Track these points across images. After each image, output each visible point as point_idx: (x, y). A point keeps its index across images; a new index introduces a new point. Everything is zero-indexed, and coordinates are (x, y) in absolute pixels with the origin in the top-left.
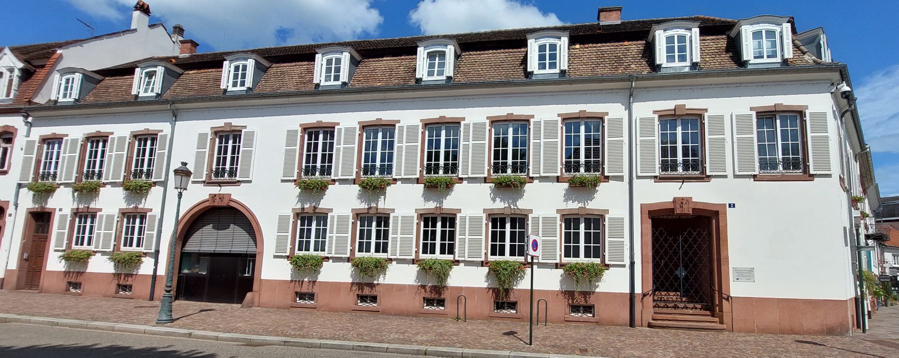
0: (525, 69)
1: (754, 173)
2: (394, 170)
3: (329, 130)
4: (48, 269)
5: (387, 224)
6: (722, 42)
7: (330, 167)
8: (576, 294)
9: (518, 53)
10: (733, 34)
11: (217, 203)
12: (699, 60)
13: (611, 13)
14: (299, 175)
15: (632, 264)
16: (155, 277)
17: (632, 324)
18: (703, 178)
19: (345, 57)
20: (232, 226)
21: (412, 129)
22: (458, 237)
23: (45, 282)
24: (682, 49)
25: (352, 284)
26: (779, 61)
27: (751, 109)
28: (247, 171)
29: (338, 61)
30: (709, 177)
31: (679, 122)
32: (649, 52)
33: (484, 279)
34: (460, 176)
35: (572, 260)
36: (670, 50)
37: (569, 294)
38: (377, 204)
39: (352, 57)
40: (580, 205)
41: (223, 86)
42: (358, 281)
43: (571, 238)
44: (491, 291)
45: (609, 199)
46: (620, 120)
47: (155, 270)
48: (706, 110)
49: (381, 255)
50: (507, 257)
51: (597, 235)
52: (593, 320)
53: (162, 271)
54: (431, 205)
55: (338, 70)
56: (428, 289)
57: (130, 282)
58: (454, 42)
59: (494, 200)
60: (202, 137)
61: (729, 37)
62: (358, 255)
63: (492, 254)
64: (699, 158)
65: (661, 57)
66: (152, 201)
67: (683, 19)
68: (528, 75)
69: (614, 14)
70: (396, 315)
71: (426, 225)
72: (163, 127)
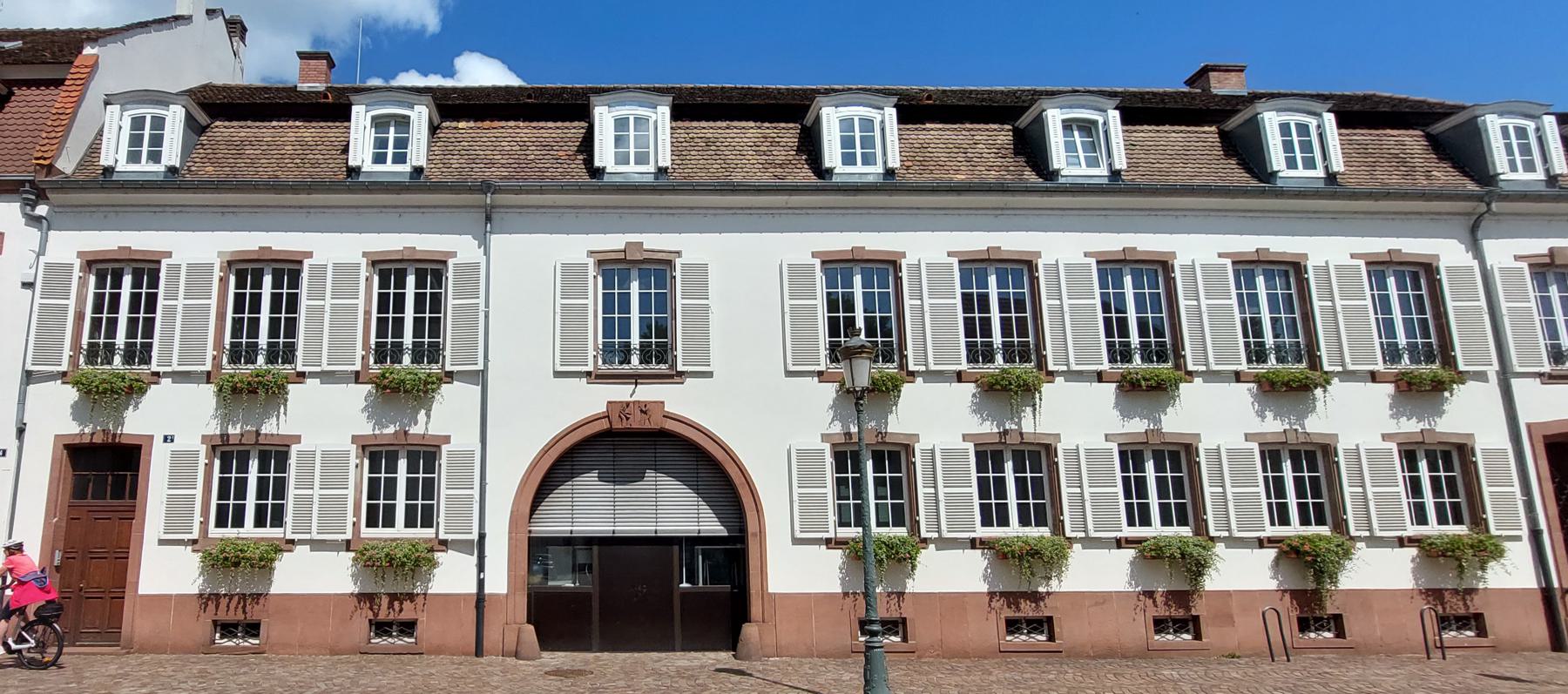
0: (589, 161)
1: (818, 368)
2: (155, 354)
3: (146, 266)
4: (774, 586)
5: (282, 465)
6: (1003, 135)
7: (148, 347)
8: (1447, 596)
9: (576, 129)
10: (1024, 120)
11: (637, 422)
12: (897, 165)
13: (1227, 75)
14: (74, 361)
15: (1535, 535)
16: (480, 599)
17: (479, 652)
18: (671, 376)
19: (175, 117)
20: (650, 474)
21: (199, 272)
22: (292, 491)
23: (134, 623)
24: (867, 142)
25: (991, 595)
26: (1106, 173)
27: (814, 255)
28: (701, 348)
29: (159, 123)
30: (681, 374)
31: (634, 273)
32: (810, 144)
33: (1269, 573)
34: (448, 368)
35: (995, 532)
36: (847, 142)
37: (1435, 595)
38: (1019, 424)
39: (189, 117)
40: (1421, 426)
41: (105, 160)
42: (1001, 588)
43: (990, 489)
44: (1287, 597)
45: (1471, 414)
46: (476, 266)
47: (481, 583)
48: (679, 253)
49: (269, 532)
50: (249, 529)
51: (897, 484)
52: (905, 647)
53: (497, 582)
54: (1138, 426)
55: (157, 141)
56: (1159, 599)
57: (254, 612)
58: (428, 99)
59: (1262, 416)
60: (798, 273)
61: (1016, 131)
62: (367, 533)
63: (368, 525)
64: (668, 340)
65: (832, 155)
66: (448, 416)
67: (1303, 96)
68: (597, 173)
69: (1233, 77)
70: (1124, 657)
71: (225, 468)
72: (460, 247)
